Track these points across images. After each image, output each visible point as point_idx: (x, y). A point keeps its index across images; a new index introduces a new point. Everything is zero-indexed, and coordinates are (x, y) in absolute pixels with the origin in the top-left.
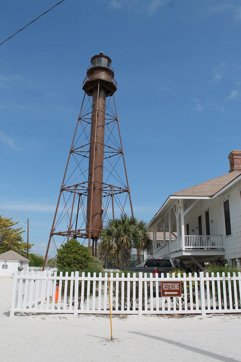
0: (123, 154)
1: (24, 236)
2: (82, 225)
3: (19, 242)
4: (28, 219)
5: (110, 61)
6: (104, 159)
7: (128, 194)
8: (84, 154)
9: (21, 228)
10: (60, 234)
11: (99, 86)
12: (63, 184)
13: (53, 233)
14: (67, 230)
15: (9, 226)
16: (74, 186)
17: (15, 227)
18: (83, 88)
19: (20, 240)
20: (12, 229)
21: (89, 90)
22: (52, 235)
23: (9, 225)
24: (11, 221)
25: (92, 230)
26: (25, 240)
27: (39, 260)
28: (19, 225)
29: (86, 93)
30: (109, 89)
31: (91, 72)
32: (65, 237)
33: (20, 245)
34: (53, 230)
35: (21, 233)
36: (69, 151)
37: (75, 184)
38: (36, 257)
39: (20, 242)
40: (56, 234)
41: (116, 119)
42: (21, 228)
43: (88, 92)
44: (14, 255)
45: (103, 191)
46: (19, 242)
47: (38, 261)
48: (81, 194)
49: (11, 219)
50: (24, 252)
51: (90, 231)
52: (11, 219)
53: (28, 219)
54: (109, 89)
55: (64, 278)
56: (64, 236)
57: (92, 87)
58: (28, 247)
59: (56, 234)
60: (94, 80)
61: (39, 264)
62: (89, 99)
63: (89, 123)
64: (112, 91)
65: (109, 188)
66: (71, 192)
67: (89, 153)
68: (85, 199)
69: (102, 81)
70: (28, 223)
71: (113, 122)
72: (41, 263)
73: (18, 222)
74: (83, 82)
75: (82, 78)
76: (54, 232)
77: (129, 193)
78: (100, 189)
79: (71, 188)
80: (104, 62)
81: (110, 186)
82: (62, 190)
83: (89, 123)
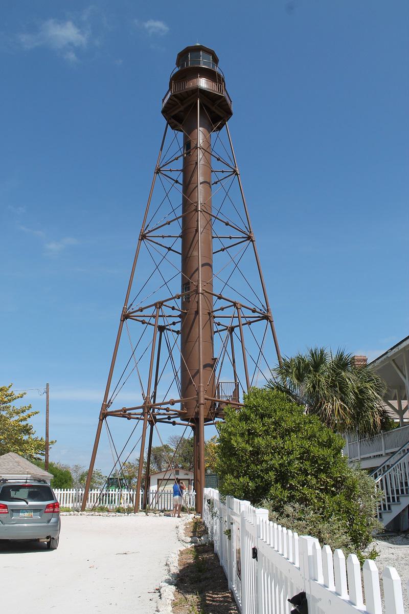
0: (252, 241)
1: (37, 425)
2: (169, 392)
3: (25, 437)
4: (48, 385)
5: (216, 60)
6: (214, 253)
7: (269, 323)
8: (168, 242)
9: (30, 407)
10: (124, 414)
11: (194, 105)
12: (126, 304)
13: (106, 412)
14: (141, 402)
15: (5, 402)
16: (155, 305)
17: (17, 405)
18: (164, 112)
19: (27, 430)
20: (11, 408)
21: (175, 115)
22: (104, 416)
23: (6, 400)
24: (9, 392)
25: (205, 399)
26: (38, 433)
27: (62, 474)
28: (28, 394)
29: (168, 123)
30: (217, 111)
31: (180, 78)
32: (133, 422)
33: (27, 442)
34: (106, 405)
35: (29, 417)
36: (137, 236)
37: (156, 302)
38: (56, 468)
39: (27, 436)
40: (113, 414)
41: (235, 171)
42: (30, 407)
43: (173, 120)
44: (18, 463)
45: (214, 317)
46: (25, 437)
47: (61, 476)
48: (162, 329)
49: (9, 387)
50: (35, 458)
51: (202, 402)
52: (9, 387)
53: (48, 385)
54: (217, 111)
55: (70, 492)
56: (129, 419)
57: (182, 108)
58: (45, 447)
59: (113, 414)
60: (186, 92)
61: (63, 483)
62: (176, 138)
63: (177, 182)
64: (222, 116)
65: (232, 311)
66: (143, 322)
67: (180, 240)
68: (174, 339)
69: (203, 92)
70: (47, 392)
71: (231, 176)
72: (66, 482)
73: (25, 394)
74: (163, 101)
75: (160, 92)
76: (109, 410)
77: (271, 322)
78: (209, 314)
79: (145, 312)
80: (204, 62)
81: (235, 304)
82: (126, 317)
83: (177, 182)
